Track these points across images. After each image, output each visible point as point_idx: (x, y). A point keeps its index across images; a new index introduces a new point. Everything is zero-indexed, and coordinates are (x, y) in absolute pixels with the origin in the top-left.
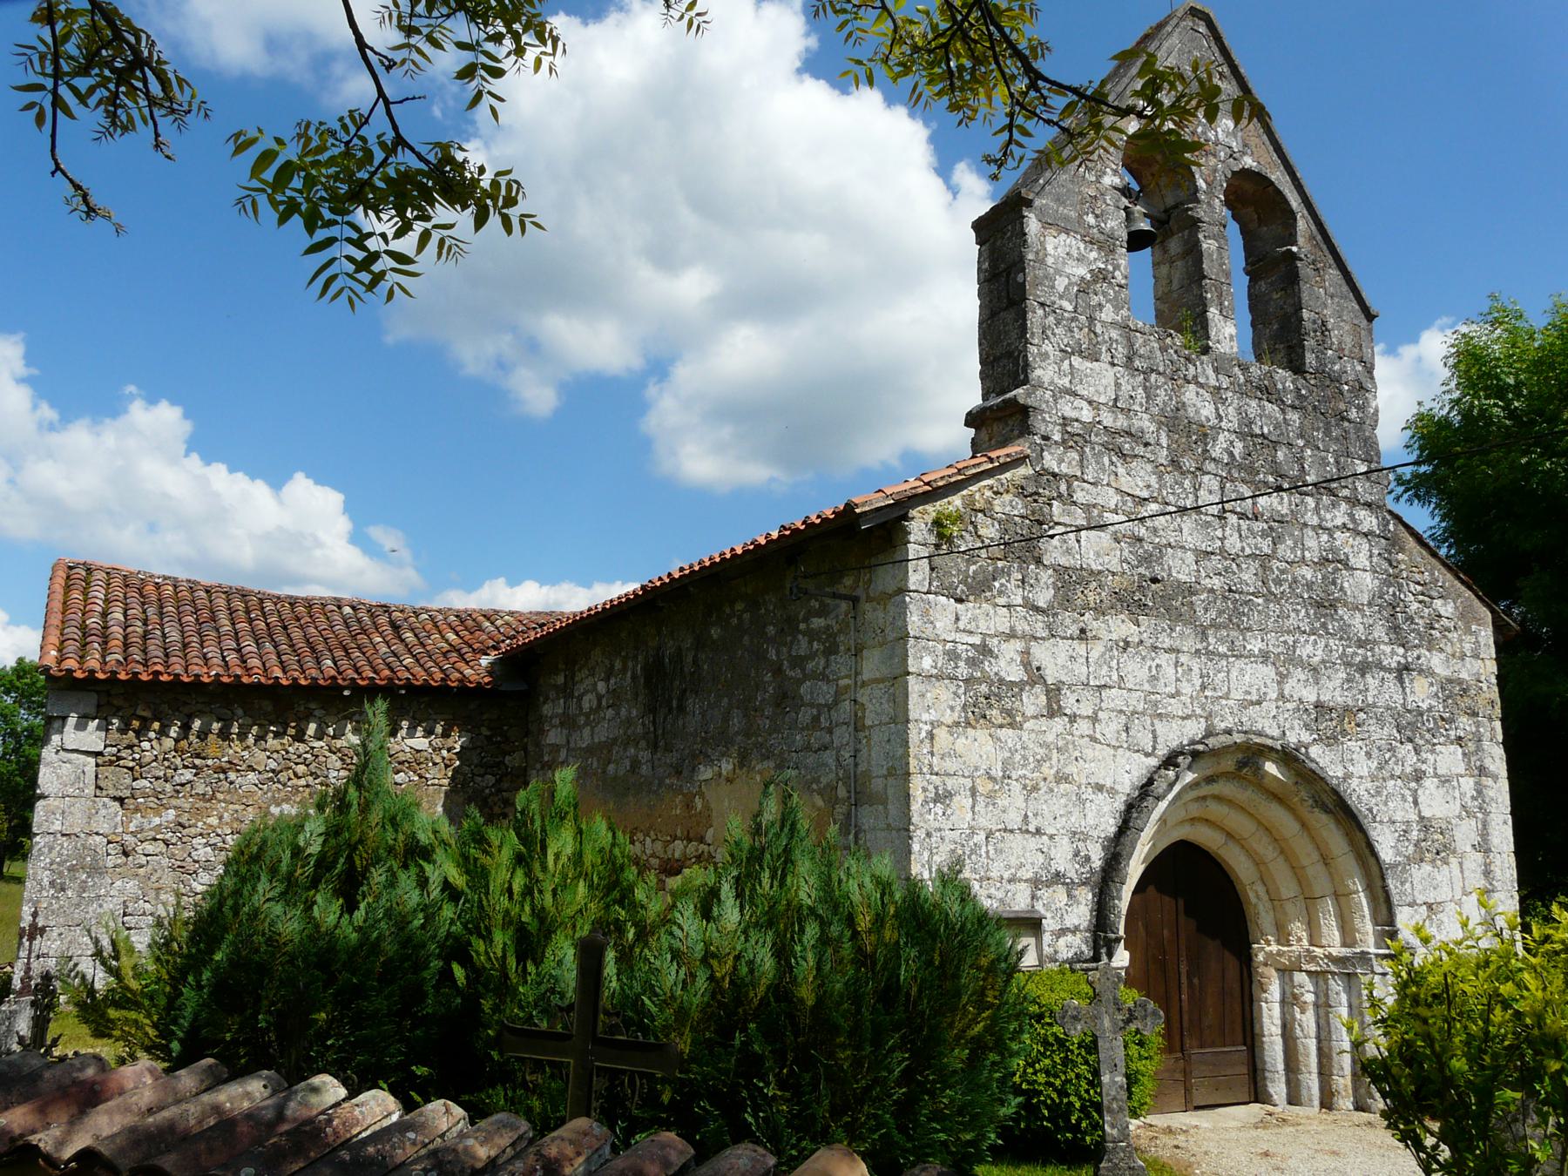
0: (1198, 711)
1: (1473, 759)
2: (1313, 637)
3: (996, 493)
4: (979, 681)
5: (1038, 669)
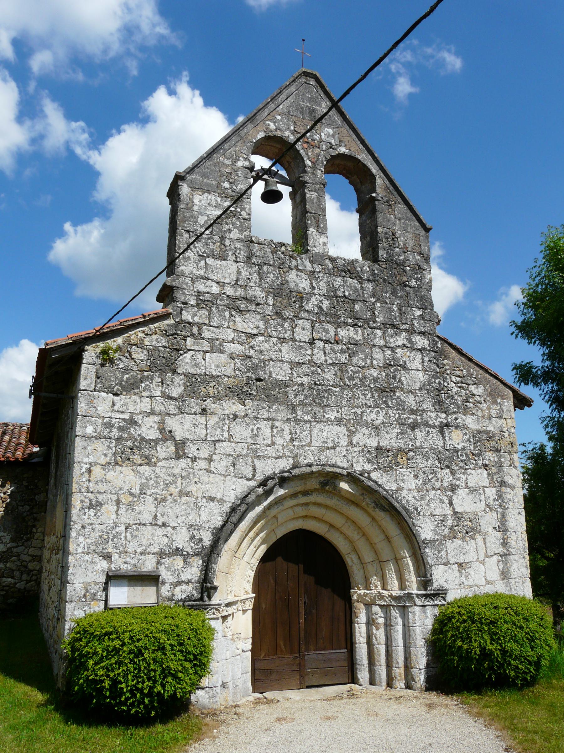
0: (287, 454)
1: (495, 477)
2: (376, 409)
3: (147, 335)
4: (126, 439)
5: (170, 432)
